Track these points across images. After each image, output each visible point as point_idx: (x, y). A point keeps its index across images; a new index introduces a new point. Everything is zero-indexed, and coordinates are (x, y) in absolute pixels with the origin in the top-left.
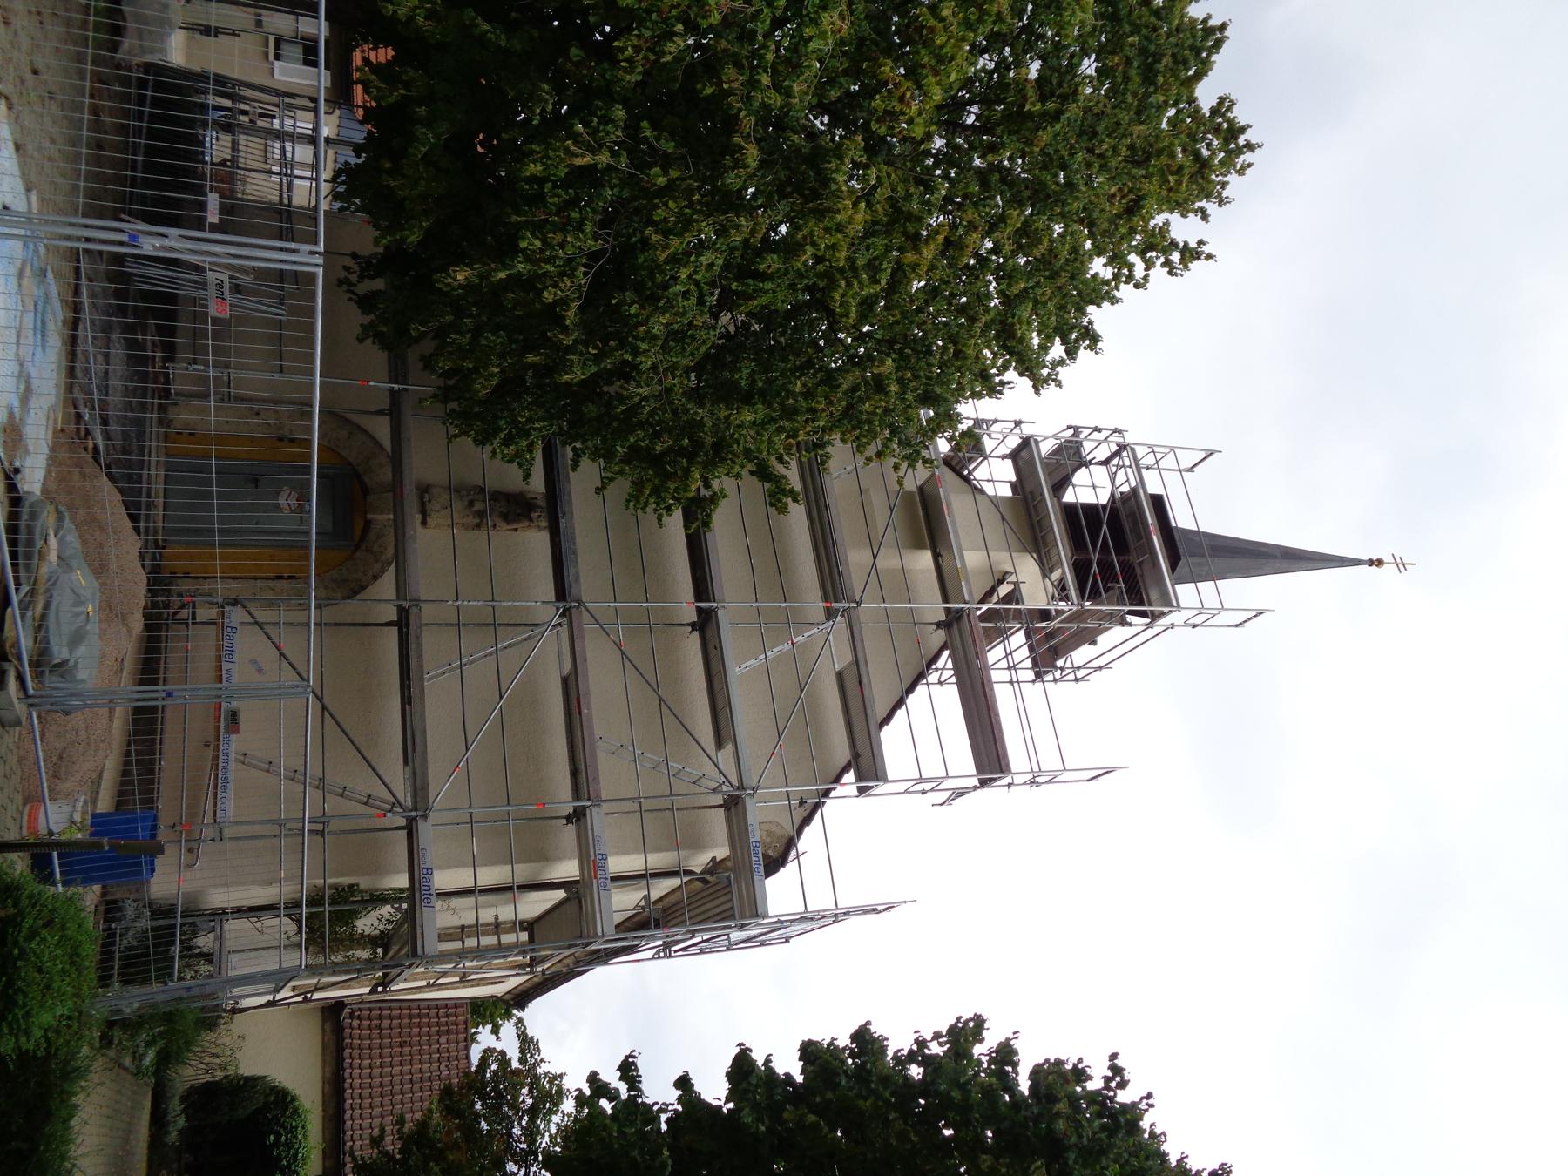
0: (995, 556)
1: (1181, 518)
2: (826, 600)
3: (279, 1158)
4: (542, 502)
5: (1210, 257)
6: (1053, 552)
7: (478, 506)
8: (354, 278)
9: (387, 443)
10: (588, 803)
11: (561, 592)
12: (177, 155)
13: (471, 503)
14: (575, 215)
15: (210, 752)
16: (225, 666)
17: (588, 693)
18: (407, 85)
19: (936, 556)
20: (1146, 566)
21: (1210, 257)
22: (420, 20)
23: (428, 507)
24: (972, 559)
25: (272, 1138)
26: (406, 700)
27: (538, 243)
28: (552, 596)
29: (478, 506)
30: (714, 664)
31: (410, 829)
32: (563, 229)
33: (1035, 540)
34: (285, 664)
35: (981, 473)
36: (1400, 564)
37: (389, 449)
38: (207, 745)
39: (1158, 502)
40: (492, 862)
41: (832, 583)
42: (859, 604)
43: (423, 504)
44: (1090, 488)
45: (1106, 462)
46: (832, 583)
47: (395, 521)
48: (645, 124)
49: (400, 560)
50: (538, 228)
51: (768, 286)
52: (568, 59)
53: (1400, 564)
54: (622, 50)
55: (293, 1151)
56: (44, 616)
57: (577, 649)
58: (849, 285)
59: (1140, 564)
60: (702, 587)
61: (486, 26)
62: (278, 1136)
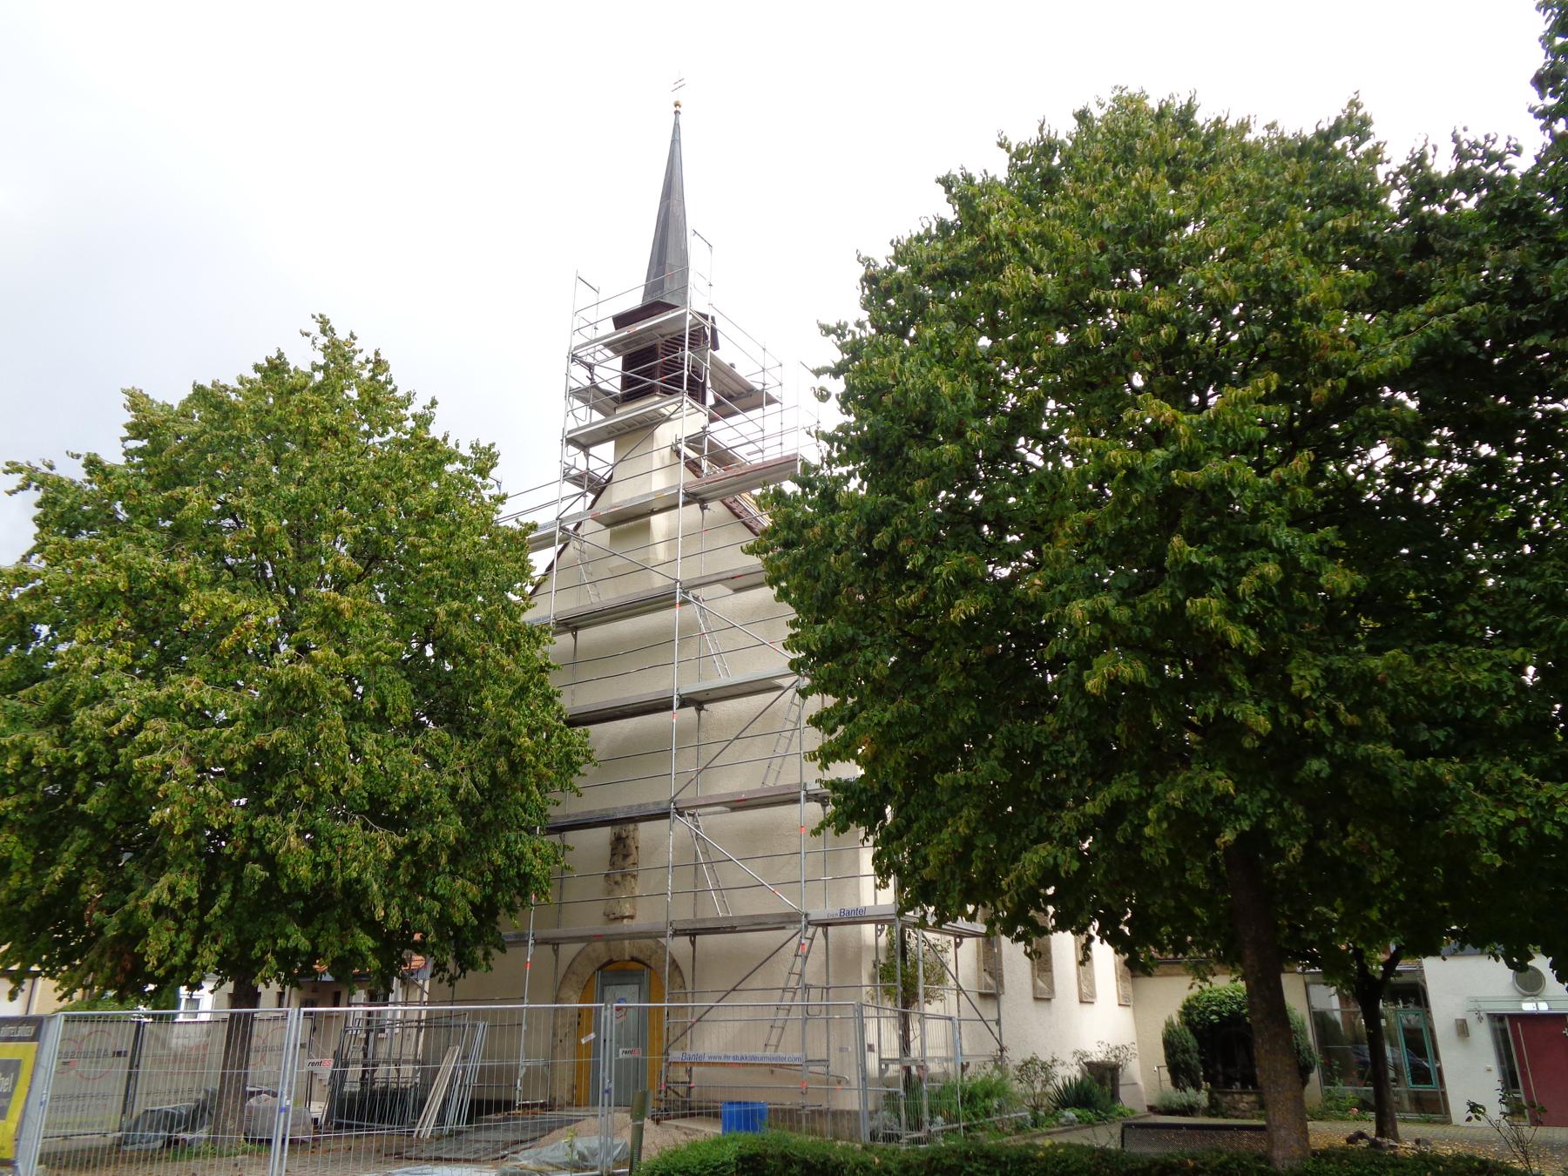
0: (657, 464)
1: (635, 301)
2: (674, 605)
3: (1232, 1012)
4: (617, 829)
5: (377, 353)
6: (650, 415)
7: (618, 878)
8: (447, 976)
9: (579, 946)
10: (803, 793)
11: (665, 815)
12: (383, 1101)
13: (616, 883)
14: (337, 841)
15: (777, 1070)
16: (706, 1060)
17: (732, 794)
18: (265, 953)
19: (653, 512)
20: (664, 331)
21: (377, 353)
22: (217, 948)
23: (617, 915)
24: (659, 483)
25: (1213, 1017)
26: (732, 930)
27: (355, 864)
28: (666, 822)
29: (618, 878)
30: (735, 691)
31: (825, 925)
32: (345, 847)
33: (646, 426)
34: (706, 1017)
35: (602, 472)
36: (679, 84)
37: (583, 945)
38: (772, 1072)
39: (621, 321)
40: (856, 862)
41: (662, 601)
42: (677, 581)
43: (616, 919)
44: (611, 374)
45: (590, 367)
46: (662, 601)
47: (630, 938)
48: (267, 803)
49: (655, 935)
50: (344, 866)
51: (390, 699)
52: (232, 854)
53: (679, 84)
54: (220, 823)
55: (1227, 1000)
56: (552, 1165)
57: (703, 802)
58: (379, 649)
59: (662, 336)
60: (662, 706)
61: (216, 907)
62: (1213, 1012)
